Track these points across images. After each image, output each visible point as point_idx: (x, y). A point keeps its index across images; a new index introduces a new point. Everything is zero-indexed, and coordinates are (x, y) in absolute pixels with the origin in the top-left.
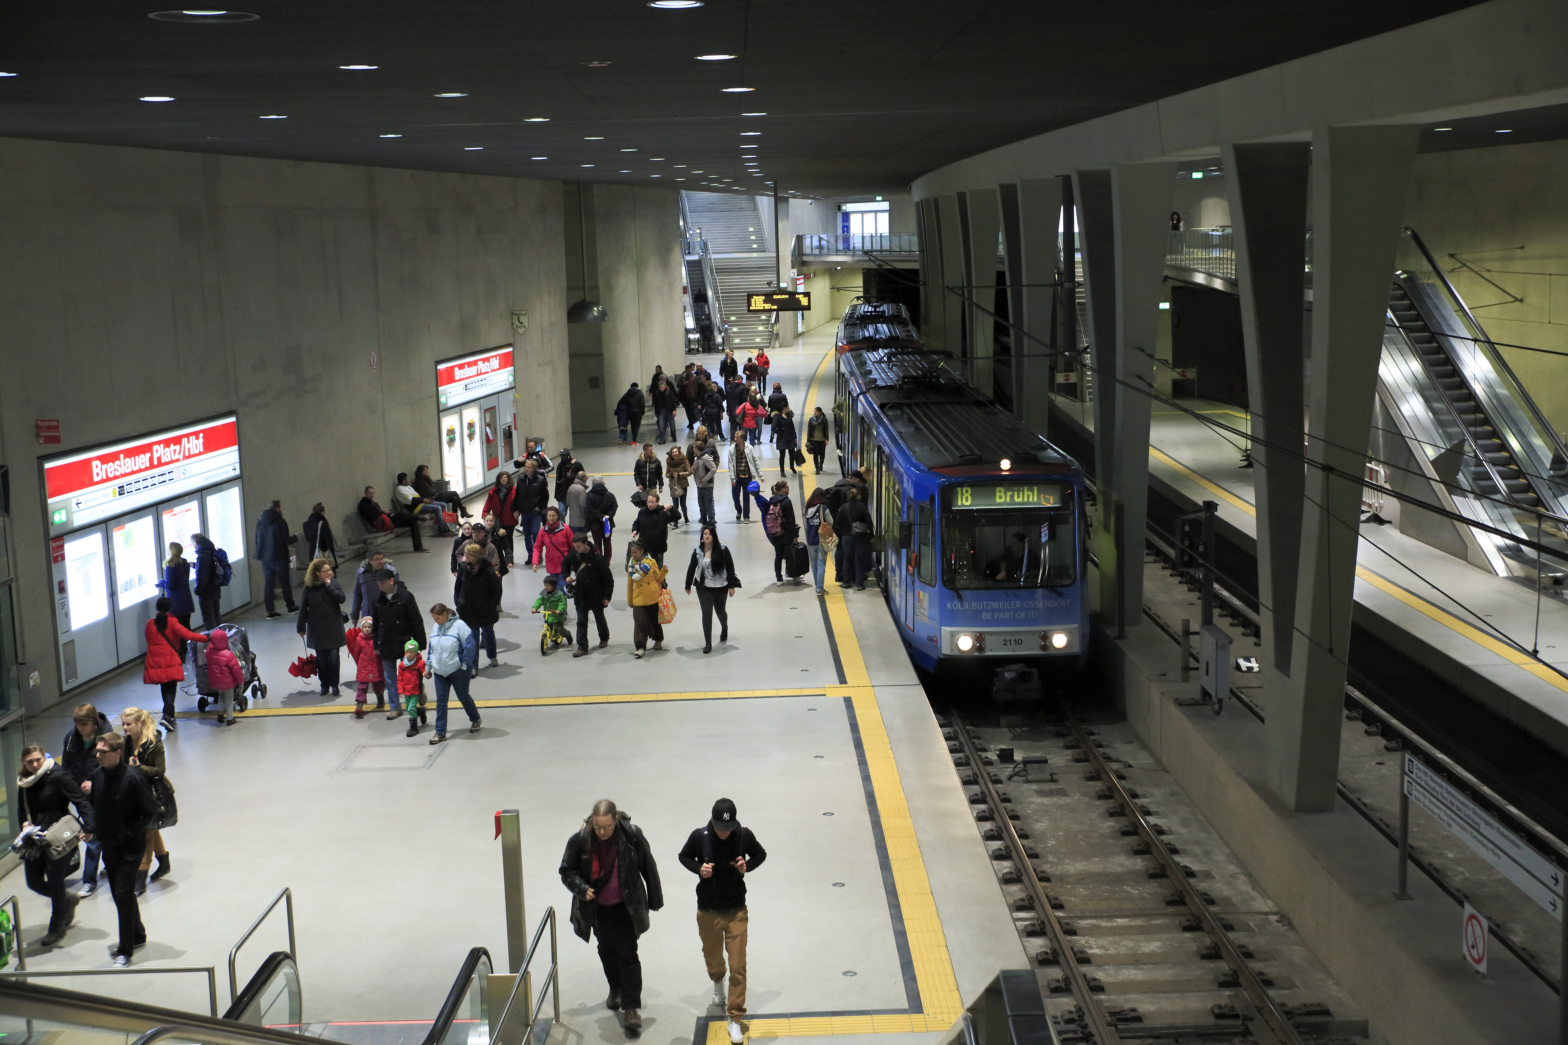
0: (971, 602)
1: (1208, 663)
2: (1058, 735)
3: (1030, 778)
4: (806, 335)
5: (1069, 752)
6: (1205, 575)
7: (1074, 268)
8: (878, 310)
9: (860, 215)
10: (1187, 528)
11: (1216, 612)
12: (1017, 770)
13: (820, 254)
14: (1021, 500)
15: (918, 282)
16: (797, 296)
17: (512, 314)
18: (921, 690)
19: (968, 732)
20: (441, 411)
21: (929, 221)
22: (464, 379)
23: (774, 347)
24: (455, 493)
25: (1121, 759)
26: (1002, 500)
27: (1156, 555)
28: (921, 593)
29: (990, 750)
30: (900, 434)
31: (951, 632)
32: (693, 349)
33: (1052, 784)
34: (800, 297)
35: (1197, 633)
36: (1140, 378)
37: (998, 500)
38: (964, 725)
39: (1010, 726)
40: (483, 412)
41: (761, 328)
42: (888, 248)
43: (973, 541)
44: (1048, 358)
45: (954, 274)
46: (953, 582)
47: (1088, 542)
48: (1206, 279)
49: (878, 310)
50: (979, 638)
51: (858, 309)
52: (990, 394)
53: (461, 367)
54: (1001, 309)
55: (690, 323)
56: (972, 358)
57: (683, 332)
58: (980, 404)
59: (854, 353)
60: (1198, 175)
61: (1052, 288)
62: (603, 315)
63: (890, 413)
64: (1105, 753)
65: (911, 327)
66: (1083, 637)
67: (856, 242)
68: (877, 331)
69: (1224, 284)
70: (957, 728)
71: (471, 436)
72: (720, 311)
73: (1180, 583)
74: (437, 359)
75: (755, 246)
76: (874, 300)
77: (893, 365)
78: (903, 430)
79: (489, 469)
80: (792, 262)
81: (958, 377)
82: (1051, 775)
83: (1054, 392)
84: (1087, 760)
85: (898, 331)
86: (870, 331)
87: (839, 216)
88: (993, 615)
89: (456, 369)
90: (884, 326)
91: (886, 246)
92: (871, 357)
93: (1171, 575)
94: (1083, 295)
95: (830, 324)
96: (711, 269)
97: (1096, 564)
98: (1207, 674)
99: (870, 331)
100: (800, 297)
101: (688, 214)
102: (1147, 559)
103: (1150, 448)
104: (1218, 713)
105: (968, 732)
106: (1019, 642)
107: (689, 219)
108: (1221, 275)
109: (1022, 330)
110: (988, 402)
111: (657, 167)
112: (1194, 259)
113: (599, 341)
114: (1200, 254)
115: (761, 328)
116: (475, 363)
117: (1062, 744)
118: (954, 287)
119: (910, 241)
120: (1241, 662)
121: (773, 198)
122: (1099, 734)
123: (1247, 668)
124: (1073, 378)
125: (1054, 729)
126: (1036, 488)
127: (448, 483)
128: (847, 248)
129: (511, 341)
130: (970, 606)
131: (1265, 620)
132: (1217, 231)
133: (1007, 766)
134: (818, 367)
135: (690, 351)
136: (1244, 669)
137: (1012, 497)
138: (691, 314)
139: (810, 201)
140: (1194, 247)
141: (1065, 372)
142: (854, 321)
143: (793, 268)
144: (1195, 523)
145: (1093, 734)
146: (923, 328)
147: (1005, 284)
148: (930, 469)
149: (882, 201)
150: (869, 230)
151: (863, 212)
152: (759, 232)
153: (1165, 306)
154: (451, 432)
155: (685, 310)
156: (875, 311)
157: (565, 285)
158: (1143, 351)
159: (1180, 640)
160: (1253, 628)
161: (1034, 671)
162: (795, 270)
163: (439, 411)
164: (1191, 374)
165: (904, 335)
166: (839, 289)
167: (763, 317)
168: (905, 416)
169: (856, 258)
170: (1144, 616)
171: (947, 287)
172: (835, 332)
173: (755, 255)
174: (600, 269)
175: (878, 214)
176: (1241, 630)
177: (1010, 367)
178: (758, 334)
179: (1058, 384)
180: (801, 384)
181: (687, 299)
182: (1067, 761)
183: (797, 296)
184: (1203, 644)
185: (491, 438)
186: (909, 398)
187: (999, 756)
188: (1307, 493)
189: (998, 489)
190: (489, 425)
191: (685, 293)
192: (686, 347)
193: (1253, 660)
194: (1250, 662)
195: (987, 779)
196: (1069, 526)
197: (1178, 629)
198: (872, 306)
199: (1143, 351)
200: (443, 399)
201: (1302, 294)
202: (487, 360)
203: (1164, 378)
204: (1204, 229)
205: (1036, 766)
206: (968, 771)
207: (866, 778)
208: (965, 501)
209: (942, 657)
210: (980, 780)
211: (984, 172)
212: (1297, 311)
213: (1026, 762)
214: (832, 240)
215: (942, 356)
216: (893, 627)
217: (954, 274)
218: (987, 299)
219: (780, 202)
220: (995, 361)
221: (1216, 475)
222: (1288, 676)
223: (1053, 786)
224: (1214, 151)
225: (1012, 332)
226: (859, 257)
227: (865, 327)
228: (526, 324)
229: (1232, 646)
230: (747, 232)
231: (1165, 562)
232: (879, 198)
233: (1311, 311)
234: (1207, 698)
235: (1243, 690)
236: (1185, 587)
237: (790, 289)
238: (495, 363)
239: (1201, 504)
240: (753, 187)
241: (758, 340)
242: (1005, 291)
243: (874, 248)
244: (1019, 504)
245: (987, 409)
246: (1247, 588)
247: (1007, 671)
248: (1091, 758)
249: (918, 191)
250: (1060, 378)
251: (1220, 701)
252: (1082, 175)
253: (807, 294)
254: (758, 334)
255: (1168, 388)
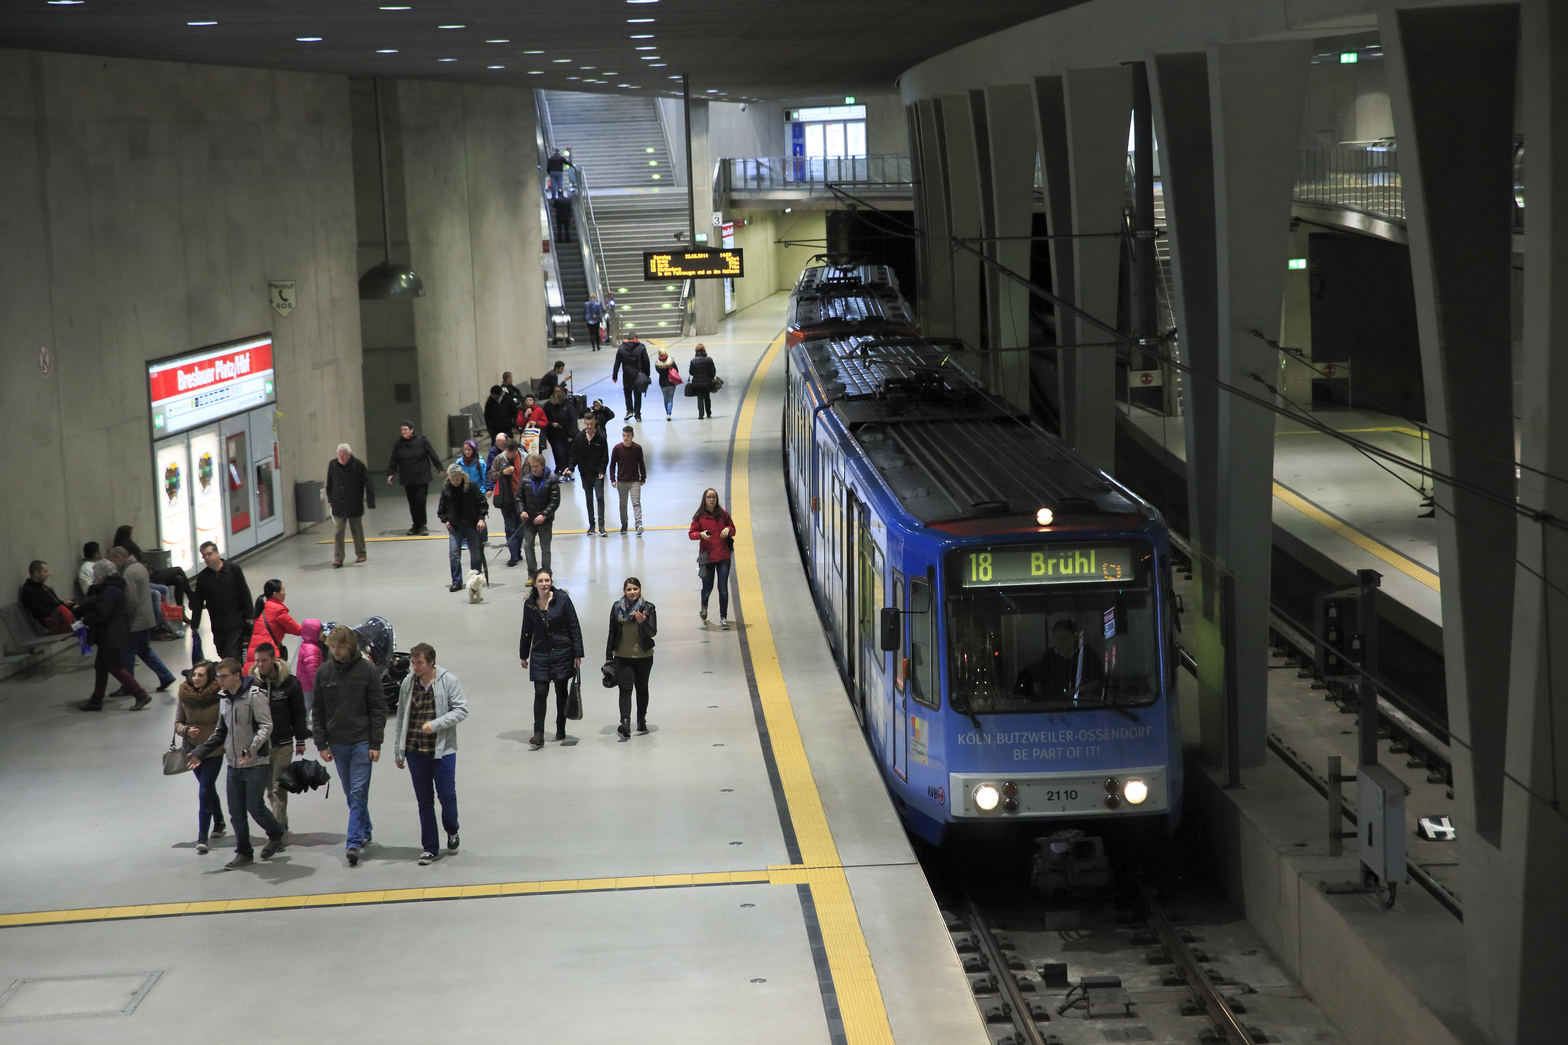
0: (996, 733)
1: (1370, 826)
2: (1138, 942)
3: (1093, 1010)
4: (738, 315)
5: (1155, 969)
6: (1364, 687)
7: (1152, 207)
8: (849, 275)
9: (821, 127)
10: (1333, 613)
11: (1384, 746)
12: (1072, 998)
13: (759, 189)
14: (1070, 571)
15: (911, 232)
16: (722, 255)
17: (270, 286)
18: (917, 874)
19: (994, 937)
20: (155, 440)
21: (927, 133)
22: (193, 389)
23: (687, 335)
24: (179, 571)
25: (1237, 979)
26: (1041, 573)
27: (1290, 656)
28: (918, 721)
29: (1030, 967)
30: (881, 470)
31: (965, 780)
32: (561, 340)
33: (1128, 1020)
34: (727, 256)
35: (1353, 779)
36: (1257, 378)
37: (1034, 573)
38: (988, 928)
39: (1061, 929)
40: (224, 441)
41: (667, 306)
42: (865, 178)
43: (998, 636)
44: (1113, 349)
45: (967, 219)
46: (968, 703)
47: (1179, 638)
48: (1363, 221)
49: (849, 275)
50: (1009, 791)
51: (818, 275)
52: (1024, 405)
53: (188, 369)
54: (1040, 273)
55: (555, 298)
56: (998, 350)
57: (543, 312)
58: (1005, 421)
59: (811, 344)
60: (1349, 58)
61: (1119, 239)
62: (416, 287)
63: (866, 438)
64: (1212, 971)
65: (901, 302)
66: (1172, 785)
67: (816, 170)
68: (848, 308)
69: (1390, 229)
70: (977, 932)
71: (205, 479)
72: (603, 279)
73: (1327, 699)
74: (150, 358)
75: (656, 177)
76: (845, 259)
77: (871, 362)
78: (885, 465)
79: (235, 532)
80: (715, 201)
81: (973, 380)
82: (1127, 1006)
83: (1126, 402)
84: (1183, 982)
85: (881, 309)
86: (837, 309)
87: (788, 130)
88: (1030, 754)
89: (180, 373)
90: (859, 300)
91: (862, 175)
92: (839, 349)
93: (1314, 687)
94: (1166, 250)
95: (774, 299)
96: (588, 214)
97: (1193, 671)
98: (1370, 843)
99: (837, 309)
100: (727, 256)
101: (550, 127)
102: (1272, 662)
103: (1275, 486)
104: (1389, 905)
105: (994, 937)
106: (1071, 795)
107: (551, 136)
108: (1386, 215)
109: (1072, 306)
110: (1019, 418)
111: (498, 53)
112: (1344, 190)
113: (409, 328)
114: (1352, 181)
115: (667, 306)
116: (211, 364)
117: (1143, 956)
118: (963, 239)
119: (899, 167)
120: (1426, 824)
121: (682, 102)
122: (1202, 940)
123: (1437, 833)
124: (1156, 378)
125: (1131, 932)
126: (1093, 553)
127: (168, 554)
128: (801, 178)
129: (269, 328)
130: (994, 738)
131: (1460, 758)
132: (1382, 145)
133: (1057, 992)
134: (757, 366)
135: (555, 343)
136: (1431, 835)
137: (1056, 567)
138: (555, 284)
139: (742, 105)
140: (1344, 172)
141: (1144, 369)
142: (812, 294)
143: (716, 210)
144: (1346, 606)
145: (1192, 940)
146: (921, 302)
147: (1045, 232)
148: (927, 525)
149: (856, 104)
150: (835, 151)
151: (825, 123)
152: (663, 154)
153: (1298, 264)
154: (172, 473)
155: (546, 278)
156: (845, 277)
157: (354, 239)
158: (1261, 335)
159: (1327, 788)
160: (1444, 770)
161: (1097, 841)
162: (720, 215)
163: (153, 441)
164: (1342, 371)
165: (889, 313)
166: (788, 244)
167: (671, 288)
168: (890, 442)
169: (814, 195)
170: (1268, 750)
171: (955, 239)
172: (784, 311)
173: (656, 190)
174: (410, 213)
175: (849, 125)
176: (1425, 773)
177: (1055, 362)
178: (662, 314)
179: (1133, 389)
180: (731, 392)
181: (550, 261)
182: (1152, 983)
183: (722, 255)
184: (1364, 796)
185: (238, 481)
186: (896, 414)
187: (1044, 976)
188: (1519, 557)
189: (1034, 555)
190: (234, 462)
191: (546, 250)
192: (549, 335)
193: (1445, 821)
194: (1441, 824)
195: (1026, 1014)
196: (1147, 612)
197: (1322, 772)
198: (841, 270)
199: (1261, 335)
200: (158, 422)
201: (1508, 243)
202: (230, 358)
203: (1297, 379)
204: (1359, 142)
205: (1103, 992)
206: (994, 1001)
207: (833, 1013)
208: (983, 574)
209: (951, 820)
210: (1014, 1015)
211: (1013, 58)
212: (1502, 269)
213: (1086, 985)
214: (778, 166)
215: (947, 347)
216: (875, 773)
217: (967, 219)
218: (1018, 258)
219: (693, 107)
220: (1031, 353)
221: (1380, 528)
222: (1498, 845)
223: (1130, 1024)
224: (1368, 21)
225: (1057, 309)
226: (820, 192)
227: (830, 303)
228: (292, 300)
229: (1408, 799)
230: (661, 155)
231: (1303, 667)
232: (850, 100)
233: (1522, 269)
234: (1372, 881)
235: (1430, 869)
236: (1332, 708)
237: (712, 244)
238: (243, 363)
239: (1355, 573)
240: (652, 85)
241: (663, 324)
242: (1046, 243)
243: (844, 179)
244: (1067, 577)
245: (1017, 430)
246: (1431, 707)
247: (1055, 841)
248: (1190, 978)
249: (911, 89)
250: (1135, 380)
251: (1392, 886)
252: (1163, 62)
253: (737, 252)
254: (662, 314)
255: (1306, 391)
